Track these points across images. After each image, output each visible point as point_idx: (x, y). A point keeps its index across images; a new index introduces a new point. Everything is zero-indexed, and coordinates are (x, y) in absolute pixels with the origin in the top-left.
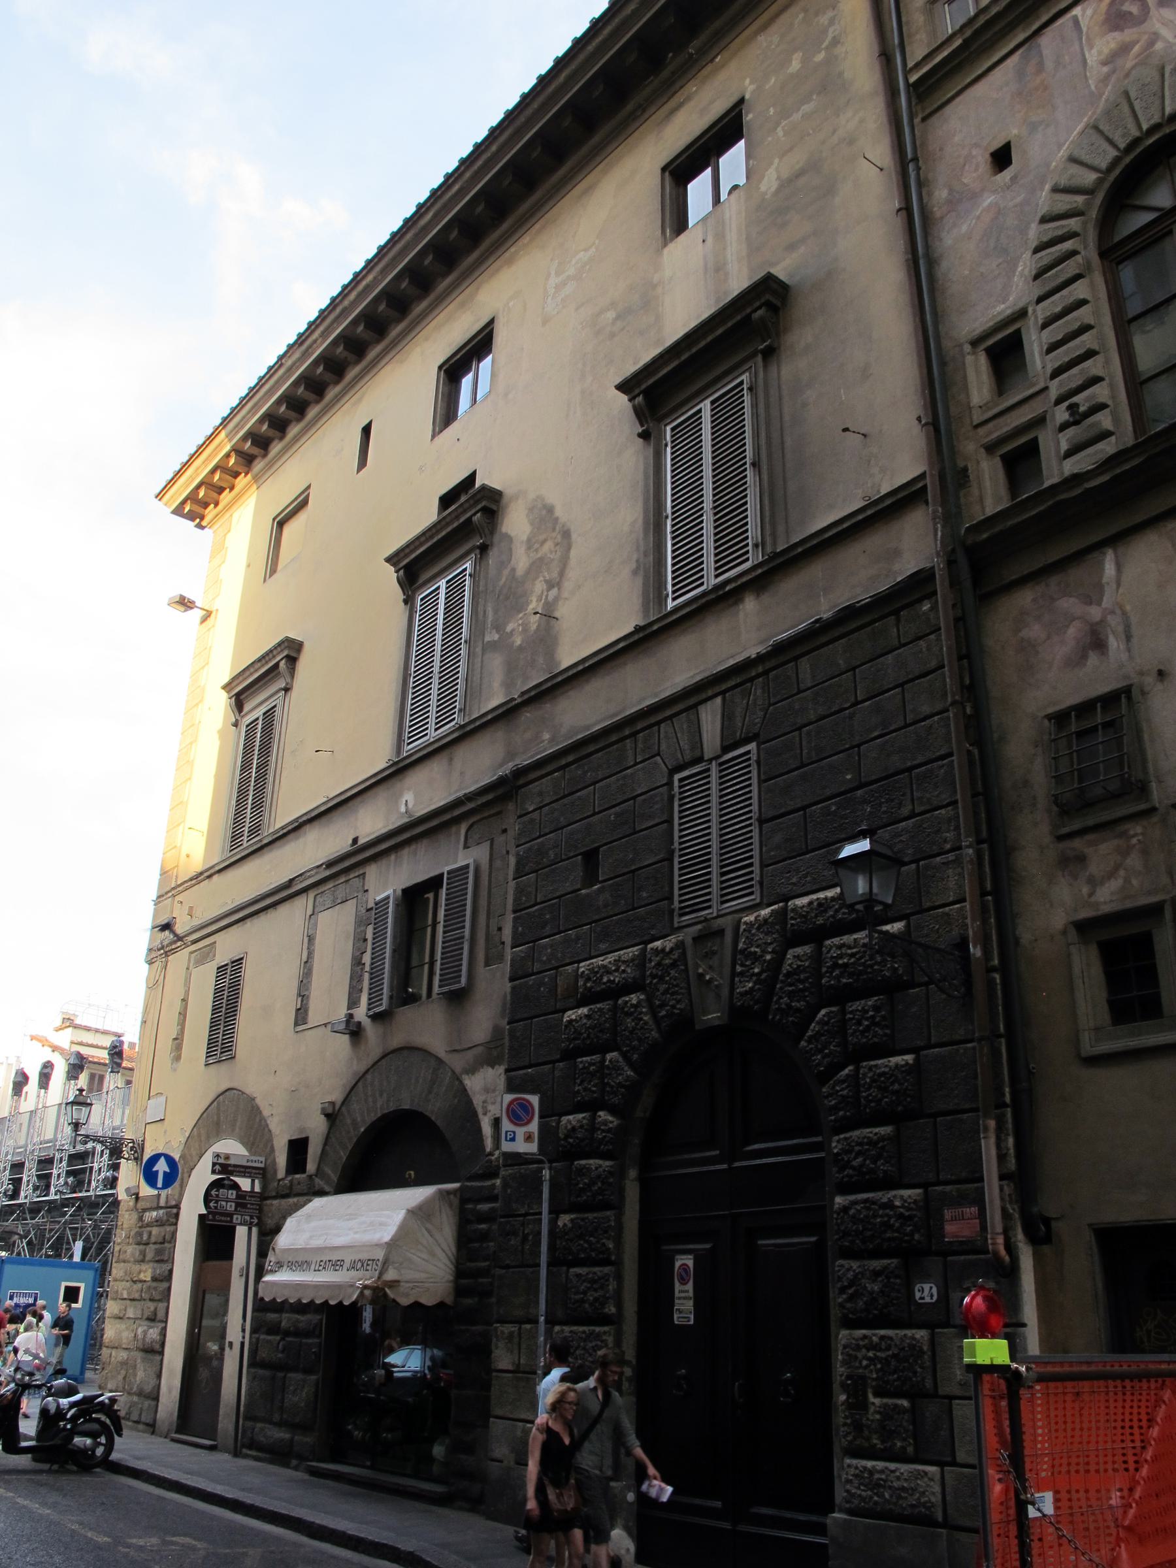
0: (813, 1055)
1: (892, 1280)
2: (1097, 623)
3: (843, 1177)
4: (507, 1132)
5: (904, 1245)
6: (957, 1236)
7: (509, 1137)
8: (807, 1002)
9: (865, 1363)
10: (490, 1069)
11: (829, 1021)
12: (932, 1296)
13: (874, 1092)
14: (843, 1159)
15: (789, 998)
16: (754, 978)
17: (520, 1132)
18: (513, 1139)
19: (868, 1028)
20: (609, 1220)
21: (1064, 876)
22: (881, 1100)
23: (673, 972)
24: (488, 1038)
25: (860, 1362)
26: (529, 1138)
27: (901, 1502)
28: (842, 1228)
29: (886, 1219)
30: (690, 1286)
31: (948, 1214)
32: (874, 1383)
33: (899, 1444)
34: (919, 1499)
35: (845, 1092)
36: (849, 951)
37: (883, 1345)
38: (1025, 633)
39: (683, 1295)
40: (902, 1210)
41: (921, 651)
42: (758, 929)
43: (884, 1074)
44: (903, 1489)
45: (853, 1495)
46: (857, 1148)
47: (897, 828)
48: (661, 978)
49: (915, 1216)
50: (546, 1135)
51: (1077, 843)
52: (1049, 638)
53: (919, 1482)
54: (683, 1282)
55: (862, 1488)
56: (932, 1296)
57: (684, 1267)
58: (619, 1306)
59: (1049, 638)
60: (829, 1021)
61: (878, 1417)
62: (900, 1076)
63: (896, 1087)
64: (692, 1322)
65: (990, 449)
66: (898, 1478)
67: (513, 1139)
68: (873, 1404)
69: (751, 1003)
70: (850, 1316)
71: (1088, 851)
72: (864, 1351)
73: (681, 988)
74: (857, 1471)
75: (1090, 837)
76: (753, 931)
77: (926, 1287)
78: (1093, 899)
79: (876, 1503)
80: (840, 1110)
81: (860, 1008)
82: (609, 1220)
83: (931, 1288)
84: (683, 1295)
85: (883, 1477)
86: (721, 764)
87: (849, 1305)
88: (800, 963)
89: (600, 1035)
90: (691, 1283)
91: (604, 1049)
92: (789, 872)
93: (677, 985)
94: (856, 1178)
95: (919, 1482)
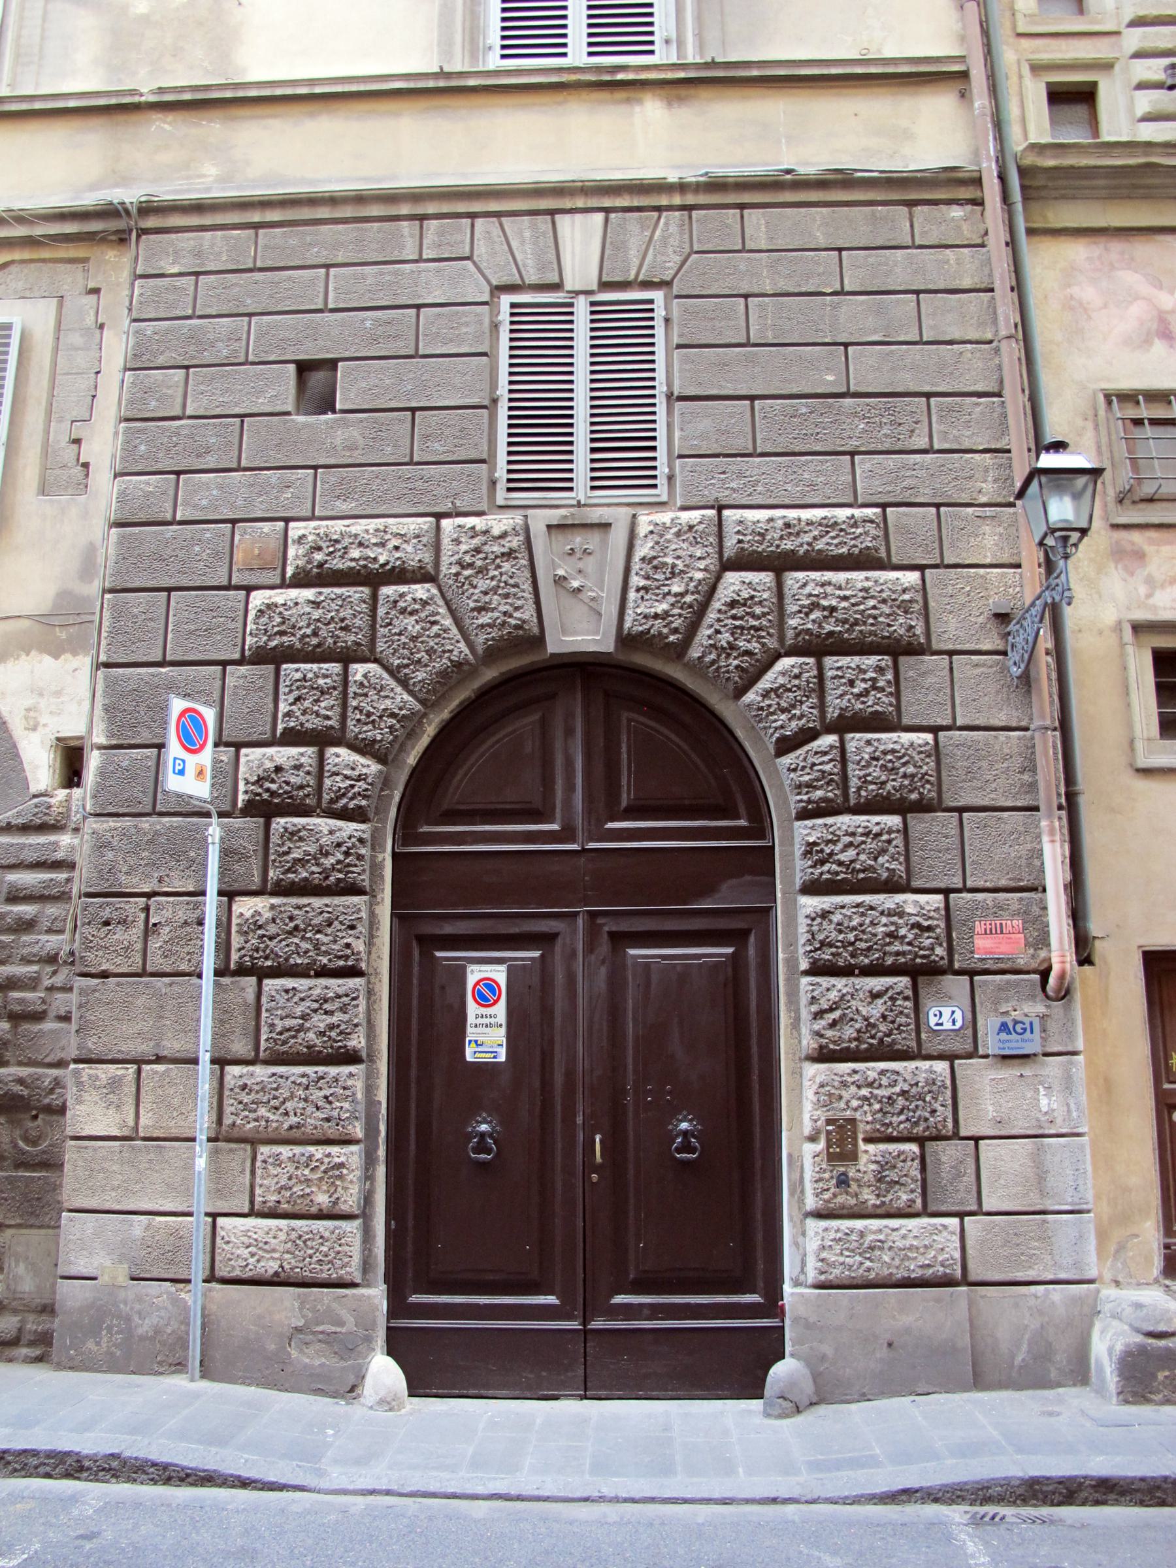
0: (773, 714)
1: (899, 1002)
2: (1167, 312)
3: (822, 874)
4: (175, 759)
5: (918, 960)
6: (991, 953)
7: (178, 768)
8: (763, 645)
9: (855, 1103)
10: (47, 659)
11: (801, 673)
12: (954, 1022)
13: (875, 772)
14: (822, 851)
15: (732, 634)
16: (672, 599)
17: (192, 761)
18: (182, 772)
19: (866, 693)
20: (360, 910)
21: (1116, 568)
22: (884, 783)
23: (506, 566)
24: (45, 608)
25: (848, 1102)
26: (200, 773)
27: (907, 1264)
28: (821, 937)
29: (893, 928)
30: (500, 1011)
31: (979, 927)
32: (868, 1127)
33: (905, 1197)
34: (934, 1257)
35: (827, 768)
36: (838, 592)
37: (885, 1081)
38: (1075, 290)
39: (480, 1021)
40: (918, 918)
41: (947, 262)
42: (678, 534)
43: (893, 751)
44: (911, 1248)
45: (833, 1265)
46: (848, 839)
47: (908, 459)
48: (482, 571)
49: (938, 926)
50: (225, 776)
51: (1136, 537)
52: (1105, 306)
53: (935, 1237)
54: (483, 1001)
55: (847, 1253)
56: (954, 1022)
57: (490, 984)
58: (371, 1036)
59: (1105, 306)
60: (801, 673)
61: (874, 1167)
62: (917, 758)
63: (911, 769)
64: (502, 1058)
65: (1037, 68)
66: (904, 1237)
67: (182, 772)
68: (866, 1152)
69: (665, 631)
70: (831, 1046)
71: (1149, 549)
72: (853, 1089)
73: (524, 591)
74: (839, 1235)
75: (1152, 534)
76: (668, 536)
77: (946, 1012)
78: (1151, 601)
79: (869, 1270)
80: (816, 788)
81: (853, 665)
82: (360, 910)
83: (953, 1012)
84: (480, 1021)
85: (882, 1237)
86: (593, 304)
87: (829, 1033)
88: (753, 593)
89: (342, 634)
90: (502, 1005)
91: (346, 657)
92: (724, 473)
93: (516, 586)
94: (843, 876)
95: (935, 1237)
